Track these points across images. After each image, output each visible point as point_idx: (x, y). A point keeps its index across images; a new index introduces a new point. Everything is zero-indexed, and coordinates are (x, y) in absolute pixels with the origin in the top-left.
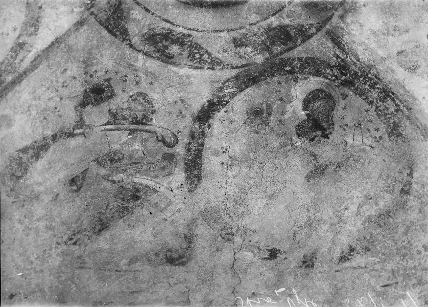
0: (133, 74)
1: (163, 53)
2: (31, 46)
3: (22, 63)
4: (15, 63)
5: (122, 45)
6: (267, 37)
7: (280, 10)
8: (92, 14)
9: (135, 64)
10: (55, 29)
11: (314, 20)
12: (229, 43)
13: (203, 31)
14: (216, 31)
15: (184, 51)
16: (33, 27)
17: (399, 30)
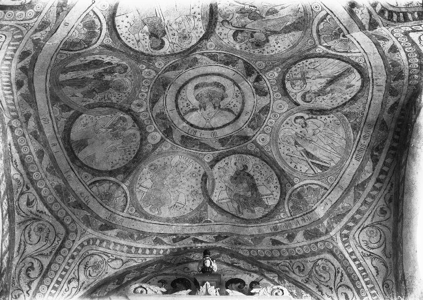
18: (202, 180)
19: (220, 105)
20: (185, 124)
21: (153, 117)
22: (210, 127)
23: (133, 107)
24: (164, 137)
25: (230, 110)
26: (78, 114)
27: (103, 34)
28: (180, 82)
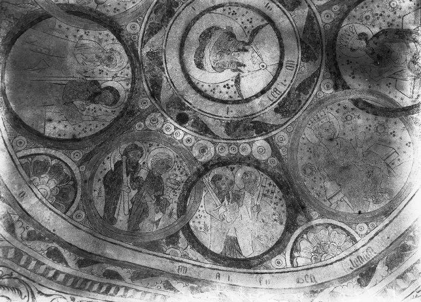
18: (362, 109)
19: (243, 42)
20: (257, 101)
21: (229, 139)
22: (276, 67)
23: (203, 159)
24: (266, 137)
25: (256, 31)
26: (187, 229)
27: (63, 157)
28: (181, 84)
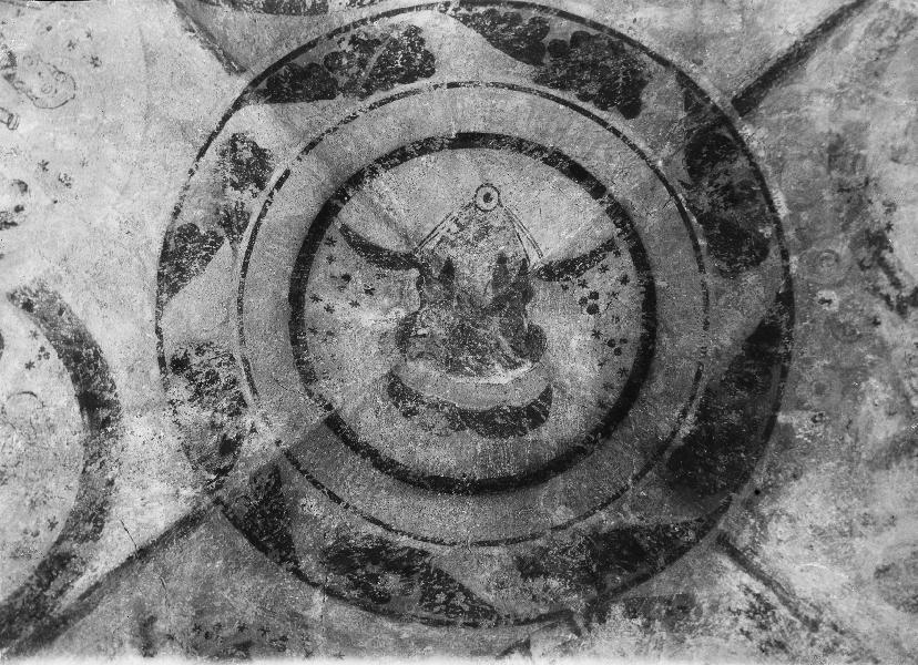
0: (299, 635)
1: (367, 590)
2: (84, 563)
3: (60, 599)
4: (46, 597)
5: (278, 571)
6: (592, 555)
7: (617, 496)
8: (218, 501)
9: (306, 613)
10: (138, 530)
11: (691, 514)
12: (509, 569)
13: (455, 544)
14: (482, 544)
15: (411, 586)
16: (92, 524)
17: (874, 523)
25: (371, 252)
28: (621, 460)
